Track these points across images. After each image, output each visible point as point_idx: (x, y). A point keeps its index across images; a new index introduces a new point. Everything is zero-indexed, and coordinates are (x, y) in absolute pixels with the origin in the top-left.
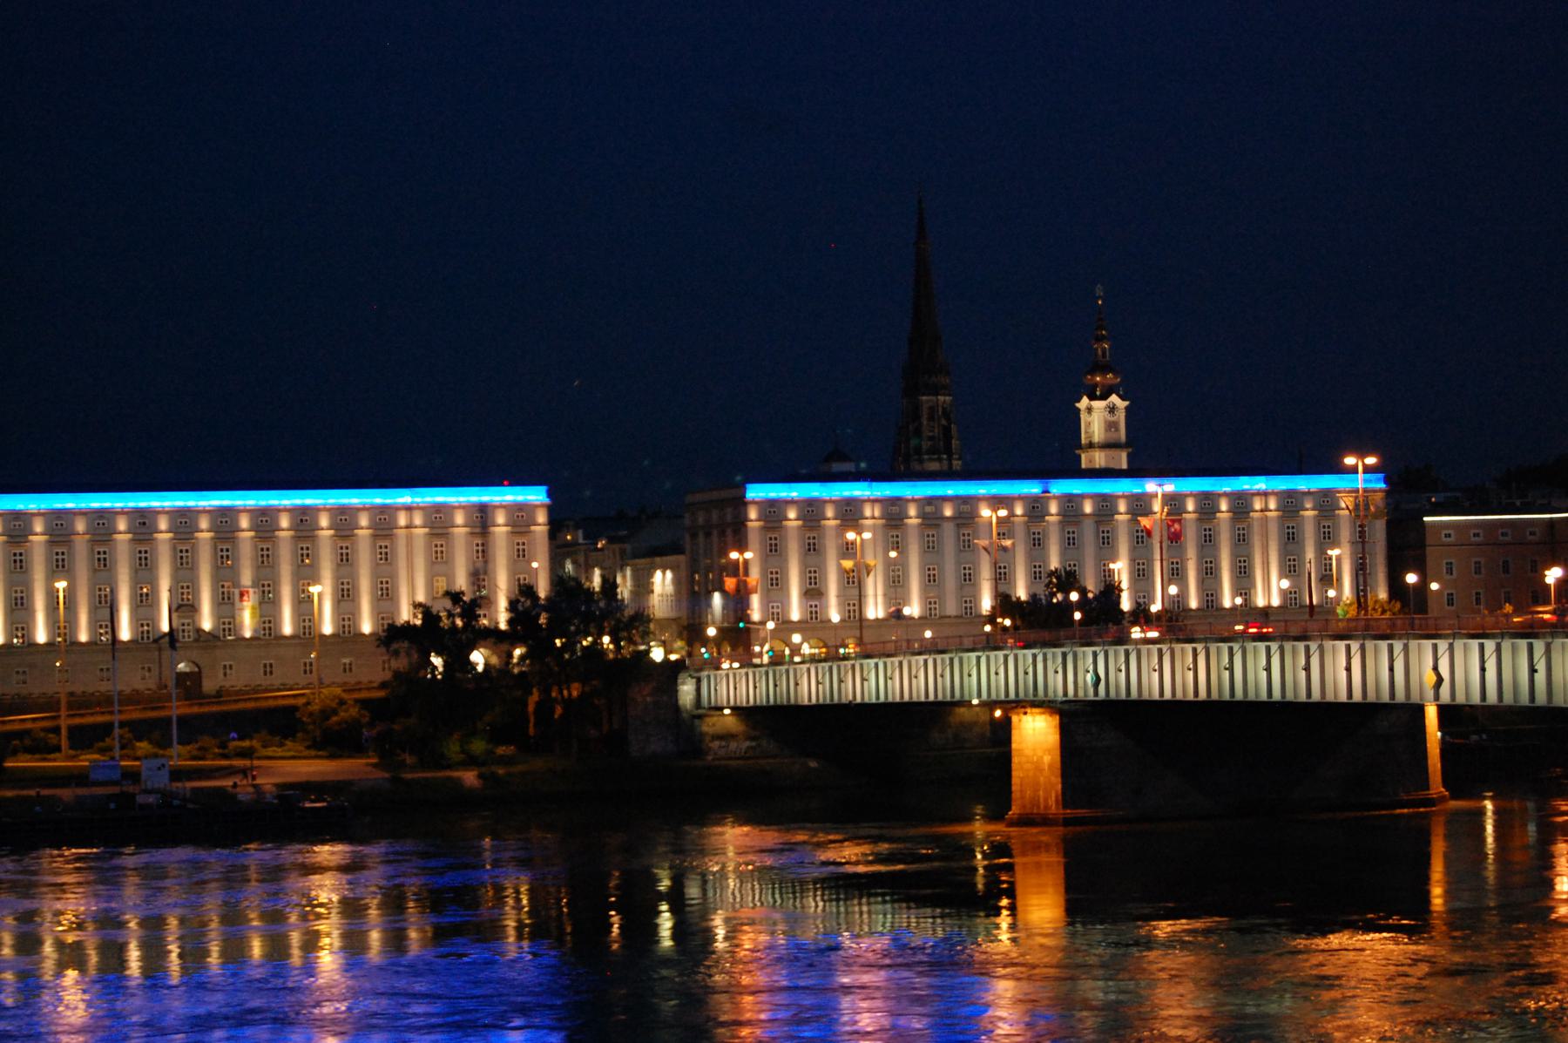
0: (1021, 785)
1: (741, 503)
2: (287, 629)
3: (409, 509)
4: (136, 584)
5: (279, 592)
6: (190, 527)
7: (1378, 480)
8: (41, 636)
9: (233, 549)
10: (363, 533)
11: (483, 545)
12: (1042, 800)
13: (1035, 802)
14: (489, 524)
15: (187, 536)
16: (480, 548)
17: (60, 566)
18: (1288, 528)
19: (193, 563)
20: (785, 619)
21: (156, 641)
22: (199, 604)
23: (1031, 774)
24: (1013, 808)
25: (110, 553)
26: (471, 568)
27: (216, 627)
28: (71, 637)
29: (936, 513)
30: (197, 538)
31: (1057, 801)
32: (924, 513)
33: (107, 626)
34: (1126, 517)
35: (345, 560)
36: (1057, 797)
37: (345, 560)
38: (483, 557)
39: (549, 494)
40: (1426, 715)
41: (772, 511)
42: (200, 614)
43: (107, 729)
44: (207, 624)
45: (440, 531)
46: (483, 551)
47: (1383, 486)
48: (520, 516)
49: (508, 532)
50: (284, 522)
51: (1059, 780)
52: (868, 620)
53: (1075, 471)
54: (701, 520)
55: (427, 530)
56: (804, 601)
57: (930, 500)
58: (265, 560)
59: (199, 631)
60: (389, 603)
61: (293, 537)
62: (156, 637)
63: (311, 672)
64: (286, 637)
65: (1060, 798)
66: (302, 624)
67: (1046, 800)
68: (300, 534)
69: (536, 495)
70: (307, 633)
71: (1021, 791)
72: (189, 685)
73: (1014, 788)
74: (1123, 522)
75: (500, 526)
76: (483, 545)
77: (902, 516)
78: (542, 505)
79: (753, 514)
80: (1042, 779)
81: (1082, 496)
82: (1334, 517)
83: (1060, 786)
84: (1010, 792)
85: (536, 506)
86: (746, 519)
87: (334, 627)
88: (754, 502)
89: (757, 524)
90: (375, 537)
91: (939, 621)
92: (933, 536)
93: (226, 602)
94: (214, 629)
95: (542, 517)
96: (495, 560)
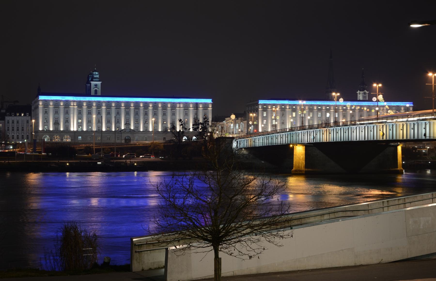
0: (296, 163)
1: (258, 104)
2: (151, 129)
3: (180, 103)
4: (144, 118)
5: (140, 121)
6: (101, 105)
7: (411, 104)
8: (123, 128)
9: (129, 111)
10: (169, 109)
11: (197, 112)
12: (300, 167)
13: (299, 167)
14: (198, 107)
15: (128, 108)
16: (196, 113)
17: (155, 115)
18: (360, 114)
19: (129, 114)
20: (82, 130)
21: (120, 131)
22: (131, 123)
23: (298, 160)
24: (294, 168)
25: (69, 110)
26: (194, 117)
27: (134, 129)
28: (91, 129)
29: (312, 108)
30: (130, 108)
31: (304, 166)
32: (310, 108)
33: (275, 129)
34: (170, 108)
35: (164, 114)
36: (304, 166)
37: (164, 114)
38: (196, 115)
39: (212, 101)
40: (398, 150)
41: (46, 103)
42: (60, 125)
43: (100, 149)
44: (132, 128)
45: (283, 110)
46: (197, 113)
47: (412, 105)
48: (205, 106)
49: (42, 107)
50: (141, 105)
51: (304, 162)
52: (103, 131)
53: (89, 95)
54: (253, 109)
55: (134, 107)
56: (54, 126)
57: (311, 105)
58: (137, 114)
59: (130, 129)
60: (91, 124)
61: (152, 109)
62: (120, 130)
63: (117, 137)
64: (141, 132)
65: (305, 166)
66: (163, 129)
67: (301, 166)
68: (145, 108)
69: (209, 101)
70: (99, 131)
71: (296, 164)
72: (128, 140)
73: (294, 163)
74: (151, 109)
75: (123, 107)
76: (197, 112)
77: (285, 108)
78: (211, 103)
79: (41, 103)
80: (300, 161)
81: (158, 103)
82: (139, 109)
83: (304, 163)
84: (293, 164)
85: (209, 103)
86: (39, 105)
87: (53, 129)
88: (260, 104)
89: (41, 106)
90: (153, 109)
91: (110, 132)
92: (284, 113)
93: (137, 122)
94: (134, 129)
95: (210, 106)
96: (199, 115)
